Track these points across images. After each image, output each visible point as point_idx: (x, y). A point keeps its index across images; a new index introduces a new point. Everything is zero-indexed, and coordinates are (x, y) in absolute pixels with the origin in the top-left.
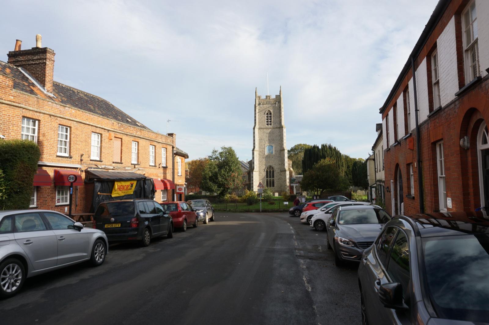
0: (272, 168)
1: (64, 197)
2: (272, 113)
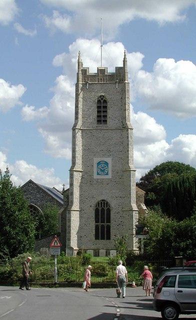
0: (107, 203)
1: (107, 222)
2: (105, 102)
